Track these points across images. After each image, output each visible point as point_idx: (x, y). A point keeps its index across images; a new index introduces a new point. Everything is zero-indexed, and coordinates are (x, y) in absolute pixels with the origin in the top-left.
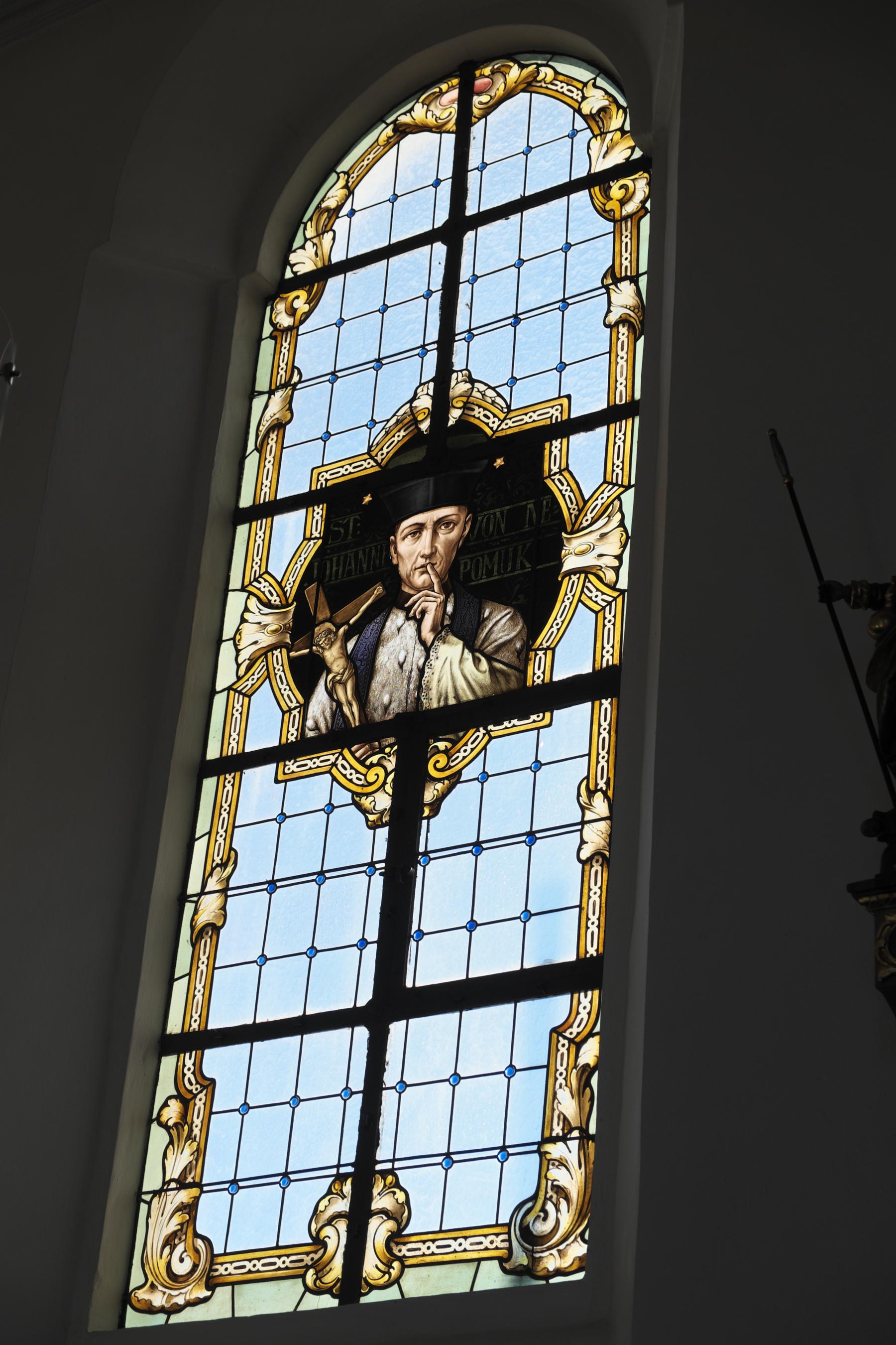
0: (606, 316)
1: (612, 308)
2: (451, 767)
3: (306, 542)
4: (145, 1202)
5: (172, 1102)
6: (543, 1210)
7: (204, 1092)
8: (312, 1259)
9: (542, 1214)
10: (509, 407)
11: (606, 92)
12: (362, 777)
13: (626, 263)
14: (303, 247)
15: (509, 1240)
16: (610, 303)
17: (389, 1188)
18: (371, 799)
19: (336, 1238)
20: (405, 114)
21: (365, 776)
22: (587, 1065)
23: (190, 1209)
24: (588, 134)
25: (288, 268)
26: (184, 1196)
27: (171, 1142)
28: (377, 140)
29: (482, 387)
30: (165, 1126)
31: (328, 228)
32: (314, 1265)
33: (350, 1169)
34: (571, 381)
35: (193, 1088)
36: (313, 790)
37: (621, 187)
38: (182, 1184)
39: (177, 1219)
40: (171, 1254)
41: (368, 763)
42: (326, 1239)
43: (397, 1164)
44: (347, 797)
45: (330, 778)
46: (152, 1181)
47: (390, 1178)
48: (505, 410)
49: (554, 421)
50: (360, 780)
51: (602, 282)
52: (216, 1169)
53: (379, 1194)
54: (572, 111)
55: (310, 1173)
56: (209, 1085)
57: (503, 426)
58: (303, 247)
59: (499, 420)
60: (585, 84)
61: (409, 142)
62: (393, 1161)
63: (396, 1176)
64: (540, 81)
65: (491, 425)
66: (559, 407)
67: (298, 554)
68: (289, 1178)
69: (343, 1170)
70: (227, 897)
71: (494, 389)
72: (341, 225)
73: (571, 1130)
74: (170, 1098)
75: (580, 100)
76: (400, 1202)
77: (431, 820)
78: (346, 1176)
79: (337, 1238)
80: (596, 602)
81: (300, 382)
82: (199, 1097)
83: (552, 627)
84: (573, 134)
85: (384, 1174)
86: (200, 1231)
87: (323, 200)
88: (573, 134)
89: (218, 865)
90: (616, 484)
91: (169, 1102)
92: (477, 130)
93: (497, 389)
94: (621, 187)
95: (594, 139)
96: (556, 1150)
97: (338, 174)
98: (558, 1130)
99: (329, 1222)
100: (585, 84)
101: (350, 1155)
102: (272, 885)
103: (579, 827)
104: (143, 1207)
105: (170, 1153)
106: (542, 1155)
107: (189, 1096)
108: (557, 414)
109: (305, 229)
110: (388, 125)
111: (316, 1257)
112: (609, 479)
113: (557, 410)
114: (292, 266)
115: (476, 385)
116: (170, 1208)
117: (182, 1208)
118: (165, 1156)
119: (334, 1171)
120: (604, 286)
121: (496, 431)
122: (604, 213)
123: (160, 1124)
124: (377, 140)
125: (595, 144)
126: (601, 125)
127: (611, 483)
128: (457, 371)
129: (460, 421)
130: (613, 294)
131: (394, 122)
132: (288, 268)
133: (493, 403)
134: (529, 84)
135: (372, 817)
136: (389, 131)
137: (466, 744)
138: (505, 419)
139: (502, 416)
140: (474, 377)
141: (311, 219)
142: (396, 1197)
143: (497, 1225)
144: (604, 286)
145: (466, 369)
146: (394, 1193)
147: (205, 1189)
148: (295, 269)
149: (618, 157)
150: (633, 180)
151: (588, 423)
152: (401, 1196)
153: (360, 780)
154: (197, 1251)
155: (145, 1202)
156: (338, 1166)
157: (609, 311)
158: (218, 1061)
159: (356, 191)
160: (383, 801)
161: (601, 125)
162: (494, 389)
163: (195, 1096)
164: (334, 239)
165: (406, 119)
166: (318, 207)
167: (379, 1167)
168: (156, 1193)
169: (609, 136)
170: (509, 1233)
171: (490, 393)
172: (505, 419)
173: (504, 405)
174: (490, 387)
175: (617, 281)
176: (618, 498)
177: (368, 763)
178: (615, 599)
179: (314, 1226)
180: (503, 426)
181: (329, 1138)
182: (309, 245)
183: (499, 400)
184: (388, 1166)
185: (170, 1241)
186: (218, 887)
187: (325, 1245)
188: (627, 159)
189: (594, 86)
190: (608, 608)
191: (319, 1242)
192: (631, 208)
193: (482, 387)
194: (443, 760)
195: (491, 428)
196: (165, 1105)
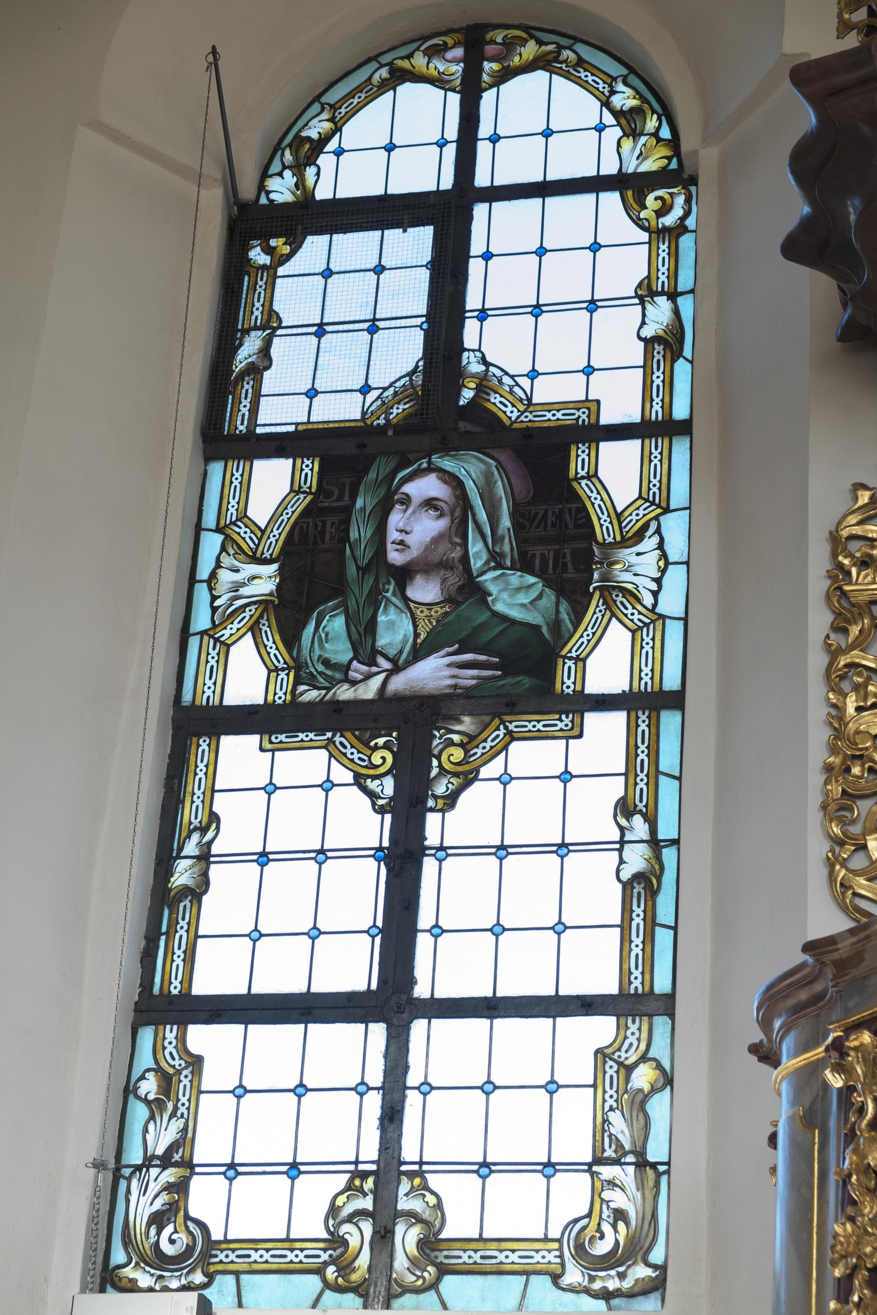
0: (641, 327)
1: (646, 320)
2: (468, 763)
3: (292, 494)
4: (125, 1178)
5: (151, 1076)
6: (599, 1229)
7: (190, 1069)
8: (331, 1256)
9: (598, 1235)
10: (529, 400)
11: (637, 92)
12: (366, 758)
13: (663, 278)
14: (280, 174)
15: (561, 1256)
16: (644, 315)
17: (417, 1190)
18: (378, 782)
19: (359, 1236)
20: (402, 58)
21: (370, 757)
22: (640, 1090)
23: (181, 1188)
24: (617, 132)
25: (263, 195)
26: (170, 1175)
27: (152, 1117)
28: (370, 78)
29: (498, 373)
30: (146, 1101)
31: (311, 159)
32: (333, 1261)
33: (374, 1167)
34: (601, 387)
35: (176, 1063)
36: (305, 763)
37: (656, 199)
38: (166, 1161)
39: (164, 1198)
40: (158, 1234)
41: (372, 744)
42: (346, 1236)
43: (425, 1167)
44: (349, 777)
45: (327, 754)
46: (135, 1156)
47: (417, 1181)
48: (526, 402)
49: (580, 423)
50: (364, 760)
51: (636, 291)
52: (208, 1148)
53: (407, 1195)
54: (599, 103)
55: (323, 1168)
56: (196, 1063)
57: (522, 418)
58: (280, 174)
59: (519, 411)
60: (614, 79)
61: (406, 90)
62: (421, 1163)
63: (424, 1179)
64: (561, 63)
65: (508, 414)
66: (587, 411)
67: (283, 505)
68: (299, 1169)
69: (361, 1167)
70: (209, 863)
71: (512, 377)
72: (326, 161)
73: (625, 1154)
74: (148, 1070)
75: (607, 94)
76: (431, 1205)
77: (355, 787)
78: (364, 1175)
79: (360, 1238)
80: (632, 620)
81: (280, 327)
82: (185, 1073)
83: (582, 636)
84: (600, 129)
85: (411, 1175)
86: (192, 1213)
87: (300, 131)
88: (600, 129)
89: (196, 829)
90: (653, 503)
91: (147, 1075)
92: (488, 98)
93: (516, 378)
94: (656, 199)
95: (625, 138)
96: (607, 1172)
97: (322, 105)
98: (609, 1153)
99: (350, 1219)
100: (614, 79)
101: (370, 1151)
102: (263, 858)
103: (617, 846)
104: (123, 1184)
105: (151, 1127)
106: (593, 1174)
107: (171, 1071)
108: (584, 417)
109: (283, 155)
110: (382, 66)
111: (335, 1254)
112: (644, 495)
113: (584, 413)
114: (268, 193)
115: (491, 369)
116: (154, 1188)
117: (168, 1188)
118: (146, 1131)
119: (352, 1167)
120: (637, 296)
121: (515, 422)
122: (638, 222)
123: (138, 1098)
124: (370, 78)
125: (627, 144)
126: (633, 126)
127: (647, 500)
128: (469, 350)
129: (472, 402)
130: (648, 306)
131: (390, 64)
132: (263, 195)
133: (511, 392)
134: (549, 63)
135: (381, 802)
136: (384, 73)
137: (485, 741)
138: (525, 411)
139: (522, 408)
140: (489, 359)
141: (290, 145)
142: (426, 1200)
143: (546, 1239)
144: (637, 296)
145: (479, 350)
146: (424, 1196)
147: (197, 1170)
148: (272, 196)
149: (650, 165)
150: (671, 194)
151: (620, 432)
152: (431, 1200)
153: (364, 760)
154: (190, 1233)
155: (125, 1178)
156: (357, 1162)
157: (643, 323)
158: (201, 1037)
159: (344, 128)
160: (388, 787)
161: (633, 126)
162: (512, 377)
163: (179, 1072)
164: (318, 174)
165: (405, 64)
166: (297, 136)
167: (404, 1168)
168: (138, 1168)
169: (643, 139)
170: (561, 1249)
171: (507, 380)
172: (525, 411)
173: (524, 397)
174: (506, 373)
175: (653, 294)
176: (656, 518)
177: (372, 744)
178: (653, 622)
179: (331, 1222)
180: (522, 418)
181: (345, 1131)
182: (287, 173)
183: (516, 389)
184: (416, 1167)
185: (158, 1220)
186: (196, 852)
187: (345, 1243)
188: (664, 168)
189: (625, 84)
190: (645, 630)
191: (336, 1241)
192: (669, 220)
193: (498, 373)
194: (458, 754)
195: (510, 418)
196: (142, 1077)
